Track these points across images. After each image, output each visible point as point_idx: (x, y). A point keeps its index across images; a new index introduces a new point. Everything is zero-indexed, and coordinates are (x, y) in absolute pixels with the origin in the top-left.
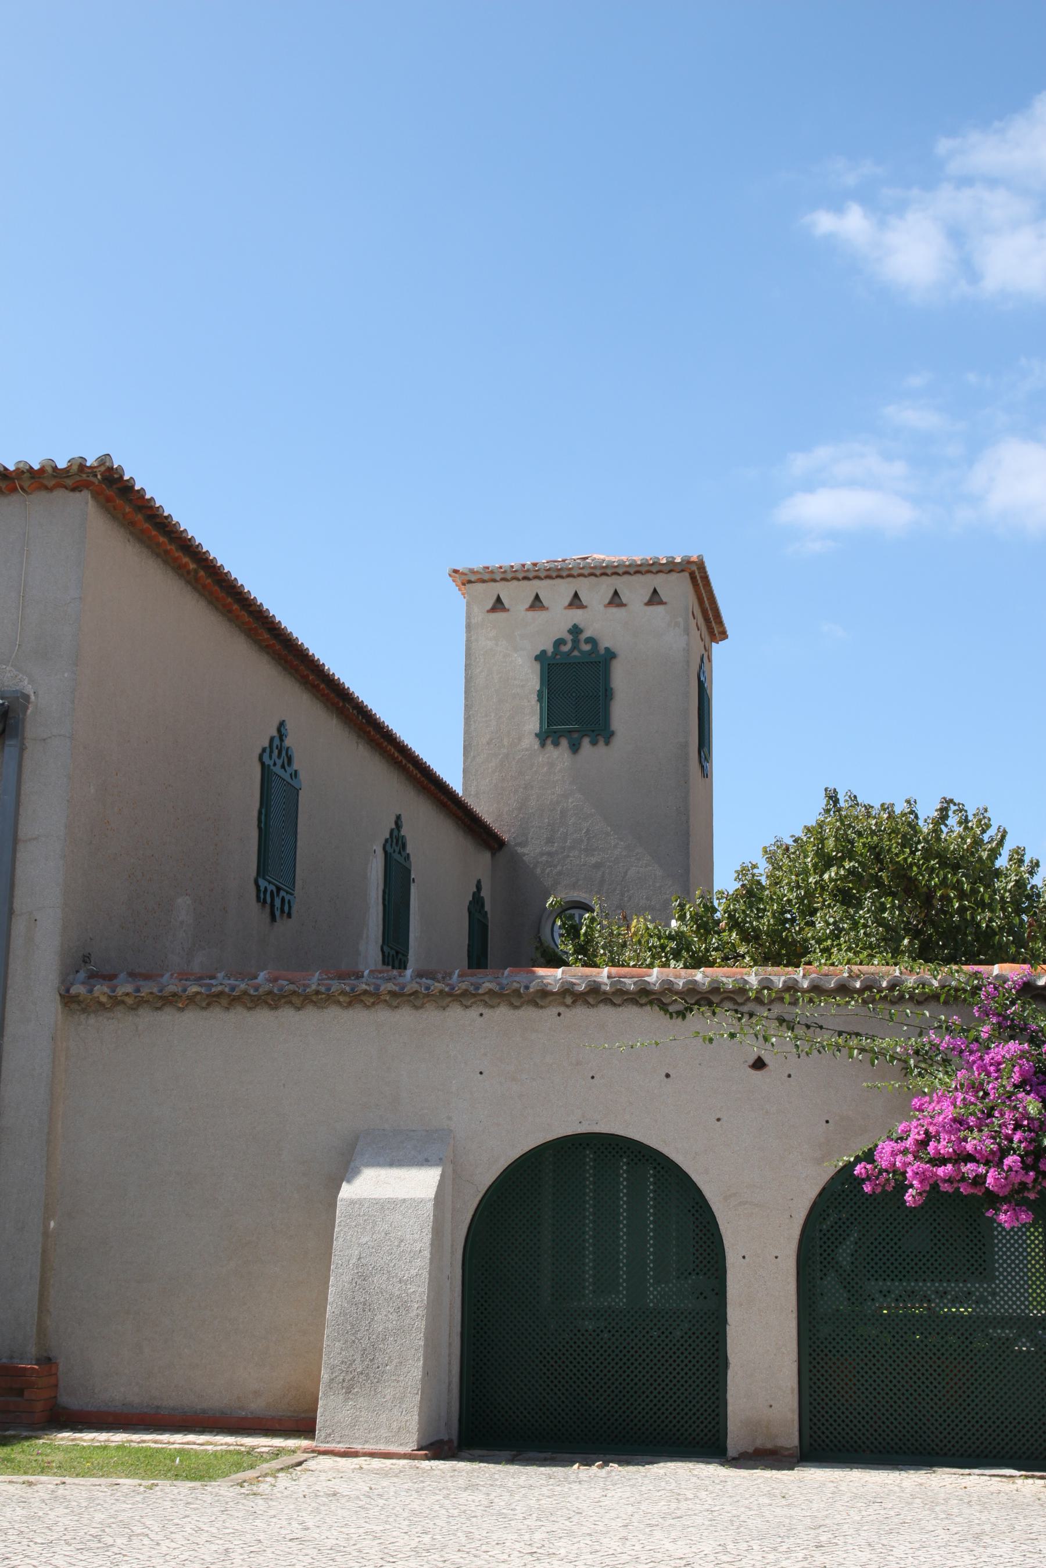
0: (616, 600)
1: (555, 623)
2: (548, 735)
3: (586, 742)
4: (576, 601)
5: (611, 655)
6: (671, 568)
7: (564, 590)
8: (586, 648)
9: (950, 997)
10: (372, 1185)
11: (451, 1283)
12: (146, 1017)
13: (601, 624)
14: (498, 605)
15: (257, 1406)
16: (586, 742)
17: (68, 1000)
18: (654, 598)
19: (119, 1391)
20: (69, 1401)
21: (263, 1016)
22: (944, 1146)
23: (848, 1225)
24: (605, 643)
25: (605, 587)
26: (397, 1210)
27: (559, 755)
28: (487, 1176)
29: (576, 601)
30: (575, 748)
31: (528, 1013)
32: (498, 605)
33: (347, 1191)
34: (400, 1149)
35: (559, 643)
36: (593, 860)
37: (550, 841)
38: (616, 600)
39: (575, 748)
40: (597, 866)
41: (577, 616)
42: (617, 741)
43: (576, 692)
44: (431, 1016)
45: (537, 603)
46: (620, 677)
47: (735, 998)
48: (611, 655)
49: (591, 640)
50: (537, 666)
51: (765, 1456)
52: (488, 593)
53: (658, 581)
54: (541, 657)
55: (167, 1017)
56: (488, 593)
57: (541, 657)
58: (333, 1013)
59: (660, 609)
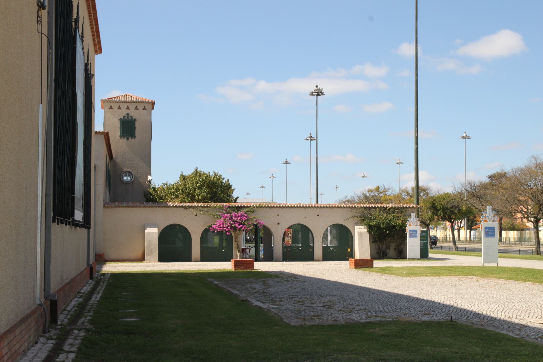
0: (136, 108)
1: (123, 112)
2: (121, 136)
3: (130, 138)
4: (128, 108)
5: (135, 120)
6: (148, 102)
7: (125, 105)
8: (130, 118)
9: (220, 208)
10: (148, 230)
11: (368, 219)
12: (115, 209)
13: (134, 113)
14: (111, 108)
15: (132, 258)
16: (130, 138)
17: (104, 207)
18: (145, 109)
19: (113, 257)
20: (106, 258)
21: (131, 209)
22: (221, 226)
23: (206, 234)
24: (134, 118)
25: (134, 106)
26: (153, 232)
27: (124, 140)
28: (161, 229)
29: (128, 108)
30: (128, 139)
31: (167, 209)
32: (111, 108)
33: (146, 231)
34: (153, 226)
35: (124, 117)
36: (132, 162)
37: (122, 158)
38: (136, 108)
39: (128, 139)
40: (132, 164)
41: (128, 111)
42: (137, 138)
43: (128, 127)
44: (154, 209)
45: (119, 108)
46: (137, 125)
47: (194, 207)
48: (135, 120)
49: (131, 117)
50: (120, 122)
51: (196, 261)
52: (109, 105)
53: (145, 105)
54: (120, 120)
55: (118, 209)
56: (109, 105)
57: (120, 120)
58: (141, 208)
59: (145, 111)
